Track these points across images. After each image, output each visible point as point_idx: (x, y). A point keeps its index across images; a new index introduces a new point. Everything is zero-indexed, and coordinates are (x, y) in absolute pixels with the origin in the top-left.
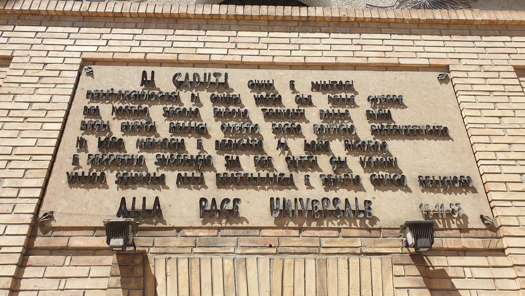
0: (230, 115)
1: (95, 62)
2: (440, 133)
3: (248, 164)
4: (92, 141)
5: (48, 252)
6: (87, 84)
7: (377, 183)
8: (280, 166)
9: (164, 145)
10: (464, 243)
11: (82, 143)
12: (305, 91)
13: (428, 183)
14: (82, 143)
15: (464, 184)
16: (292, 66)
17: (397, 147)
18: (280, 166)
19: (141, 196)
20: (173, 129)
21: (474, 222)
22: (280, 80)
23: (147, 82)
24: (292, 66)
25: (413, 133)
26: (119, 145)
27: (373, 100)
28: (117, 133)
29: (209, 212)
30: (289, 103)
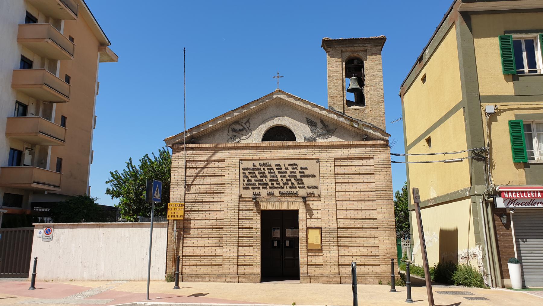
0: (271, 173)
1: (242, 160)
2: (314, 176)
3: (275, 183)
4: (246, 180)
5: (171, 271)
6: (242, 166)
7: (299, 187)
8: (281, 185)
9: (259, 180)
10: (314, 199)
11: (244, 180)
12: (287, 166)
13: (309, 187)
14: (244, 180)
15: (316, 187)
16: (284, 159)
17: (305, 180)
18: (281, 185)
19: (256, 191)
20: (261, 177)
21: (316, 195)
22: (281, 163)
23: (254, 165)
24: (284, 159)
25: (308, 176)
26: (251, 181)
27: (301, 168)
28: (250, 178)
29: (269, 194)
30: (284, 170)
